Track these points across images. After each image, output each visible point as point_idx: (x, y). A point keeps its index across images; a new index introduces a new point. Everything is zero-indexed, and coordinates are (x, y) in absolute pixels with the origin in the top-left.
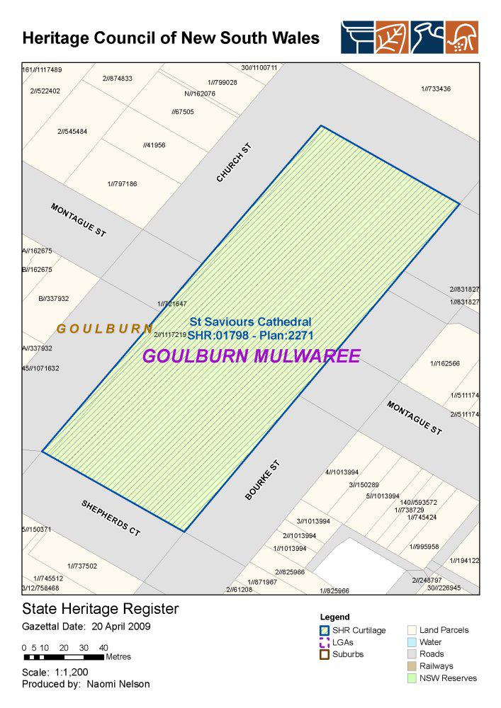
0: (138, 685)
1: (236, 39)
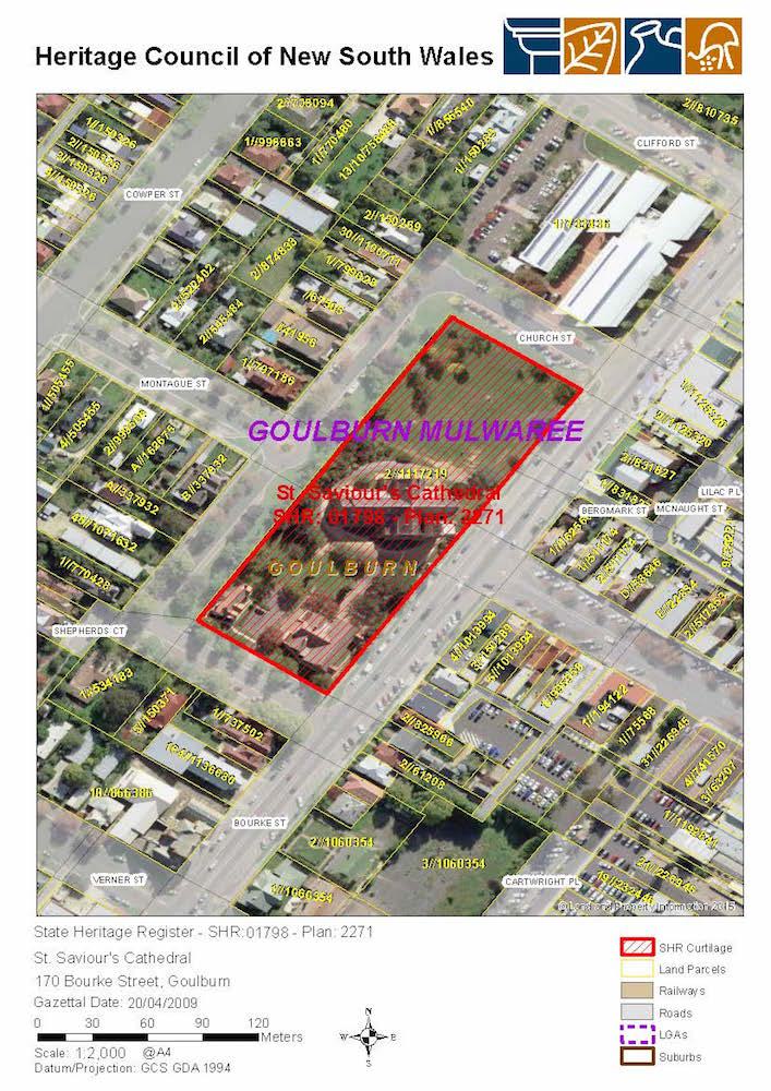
1: (364, 58)
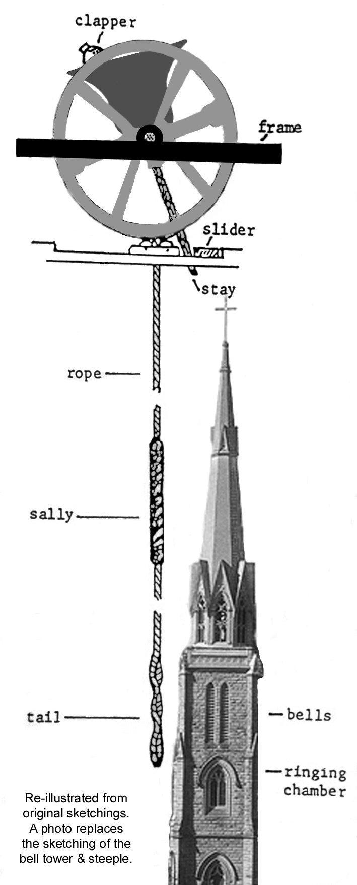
0: (226, 370)
